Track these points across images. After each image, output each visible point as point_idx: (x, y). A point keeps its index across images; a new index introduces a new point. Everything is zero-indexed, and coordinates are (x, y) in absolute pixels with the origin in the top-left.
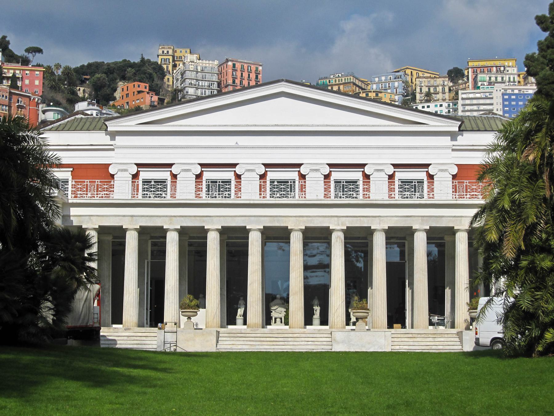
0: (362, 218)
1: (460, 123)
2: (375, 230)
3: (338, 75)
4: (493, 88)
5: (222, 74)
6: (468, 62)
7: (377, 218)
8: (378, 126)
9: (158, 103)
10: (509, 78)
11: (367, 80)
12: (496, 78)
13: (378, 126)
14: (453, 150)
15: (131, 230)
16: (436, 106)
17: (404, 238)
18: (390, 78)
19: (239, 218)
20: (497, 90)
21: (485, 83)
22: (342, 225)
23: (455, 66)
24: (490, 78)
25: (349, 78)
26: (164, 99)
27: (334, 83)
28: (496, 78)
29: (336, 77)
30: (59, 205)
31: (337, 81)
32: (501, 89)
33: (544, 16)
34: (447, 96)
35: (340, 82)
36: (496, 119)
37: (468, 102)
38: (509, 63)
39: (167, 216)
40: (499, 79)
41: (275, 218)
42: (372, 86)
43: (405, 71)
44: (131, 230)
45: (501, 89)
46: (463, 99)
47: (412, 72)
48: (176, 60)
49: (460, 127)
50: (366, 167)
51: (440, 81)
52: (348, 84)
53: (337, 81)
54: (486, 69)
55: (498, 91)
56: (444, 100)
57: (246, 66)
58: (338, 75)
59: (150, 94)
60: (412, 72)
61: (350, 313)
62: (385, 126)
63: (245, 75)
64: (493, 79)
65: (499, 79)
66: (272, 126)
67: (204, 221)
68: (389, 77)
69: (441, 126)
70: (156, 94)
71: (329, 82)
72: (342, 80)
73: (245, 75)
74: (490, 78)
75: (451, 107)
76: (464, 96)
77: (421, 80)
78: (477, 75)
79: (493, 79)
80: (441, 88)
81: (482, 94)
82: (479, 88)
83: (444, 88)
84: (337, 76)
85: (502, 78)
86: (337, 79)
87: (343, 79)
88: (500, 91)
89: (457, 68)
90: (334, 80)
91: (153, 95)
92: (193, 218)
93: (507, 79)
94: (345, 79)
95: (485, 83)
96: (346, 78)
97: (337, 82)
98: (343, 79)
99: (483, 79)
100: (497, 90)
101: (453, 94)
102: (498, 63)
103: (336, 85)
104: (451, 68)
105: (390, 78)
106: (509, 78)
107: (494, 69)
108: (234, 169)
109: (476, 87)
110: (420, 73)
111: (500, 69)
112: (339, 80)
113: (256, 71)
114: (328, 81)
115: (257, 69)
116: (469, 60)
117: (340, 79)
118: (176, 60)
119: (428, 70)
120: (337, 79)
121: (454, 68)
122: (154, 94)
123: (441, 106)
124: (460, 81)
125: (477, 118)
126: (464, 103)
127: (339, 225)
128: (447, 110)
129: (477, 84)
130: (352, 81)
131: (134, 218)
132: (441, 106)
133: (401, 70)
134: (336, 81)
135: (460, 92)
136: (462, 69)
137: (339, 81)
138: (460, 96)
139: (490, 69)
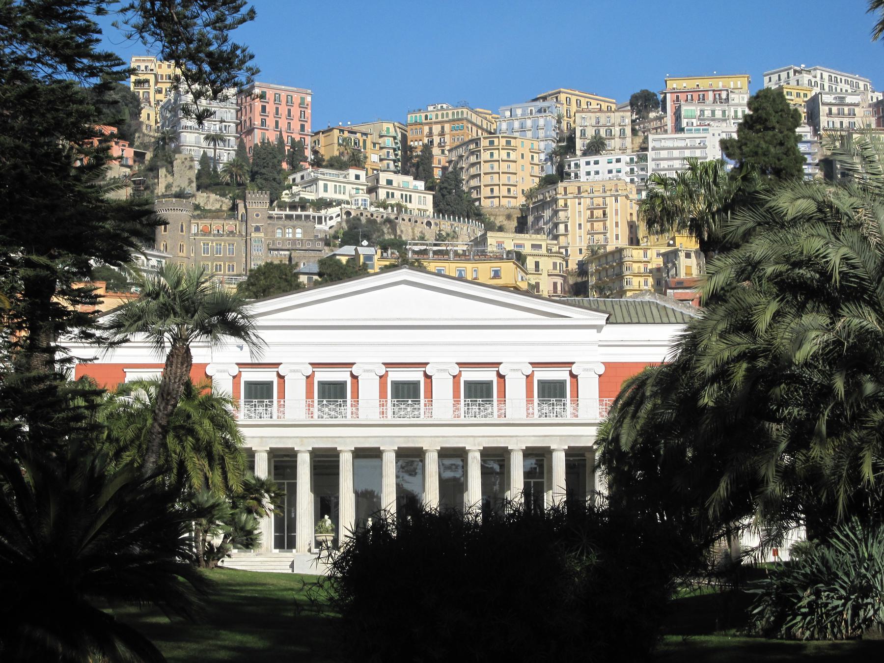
0: (499, 438)
1: (607, 316)
2: (512, 450)
3: (442, 107)
4: (708, 130)
5: (244, 110)
6: (666, 81)
7: (514, 438)
8: (514, 319)
9: (135, 161)
10: (736, 112)
11: (490, 112)
12: (713, 112)
13: (514, 319)
14: (600, 346)
15: (389, 451)
17: (543, 455)
18: (531, 111)
19: (373, 439)
20: (713, 135)
21: (694, 121)
23: (644, 88)
24: (702, 111)
25: (460, 111)
26: (144, 154)
27: (434, 120)
28: (713, 112)
29: (438, 110)
32: (720, 132)
33: (731, 140)
34: (628, 141)
35: (445, 119)
36: (651, 304)
37: (664, 154)
38: (735, 84)
39: (297, 437)
40: (719, 114)
41: (410, 439)
42: (500, 125)
43: (557, 98)
44: (389, 451)
45: (720, 132)
46: (654, 149)
47: (822, 74)
48: (160, 81)
49: (608, 319)
51: (616, 117)
52: (458, 122)
54: (695, 95)
55: (717, 135)
56: (623, 150)
57: (283, 94)
58: (442, 107)
59: (121, 144)
60: (822, 74)
63: (283, 110)
64: (708, 113)
65: (719, 114)
67: (336, 443)
68: (529, 109)
69: (586, 319)
70: (131, 145)
71: (426, 118)
72: (447, 114)
73: (283, 110)
74: (702, 111)
76: (657, 145)
78: (680, 107)
79: (708, 113)
80: (618, 129)
81: (687, 140)
82: (682, 130)
83: (624, 130)
84: (439, 107)
85: (724, 112)
86: (440, 113)
87: (450, 112)
88: (719, 135)
89: (647, 91)
90: (434, 114)
91: (124, 146)
92: (325, 439)
93: (732, 114)
94: (453, 113)
95: (694, 121)
96: (455, 111)
97: (440, 119)
99: (690, 114)
100: (713, 135)
101: (639, 140)
102: (720, 84)
103: (436, 123)
104: (637, 90)
105: (531, 111)
106: (736, 112)
107: (711, 94)
109: (679, 129)
110: (582, 99)
111: (720, 95)
112: (443, 114)
113: (300, 104)
114: (423, 115)
115: (303, 99)
116: (668, 77)
117: (445, 112)
118: (160, 81)
119: (597, 95)
120: (440, 113)
121: (643, 92)
122: (127, 145)
123: (618, 161)
124: (652, 115)
125: (629, 304)
126: (657, 157)
127: (475, 445)
128: (628, 169)
129: (680, 122)
130: (465, 116)
131: (264, 439)
133: (550, 95)
134: (437, 116)
135: (651, 137)
136: (656, 92)
137: (443, 117)
138: (651, 145)
139: (704, 95)
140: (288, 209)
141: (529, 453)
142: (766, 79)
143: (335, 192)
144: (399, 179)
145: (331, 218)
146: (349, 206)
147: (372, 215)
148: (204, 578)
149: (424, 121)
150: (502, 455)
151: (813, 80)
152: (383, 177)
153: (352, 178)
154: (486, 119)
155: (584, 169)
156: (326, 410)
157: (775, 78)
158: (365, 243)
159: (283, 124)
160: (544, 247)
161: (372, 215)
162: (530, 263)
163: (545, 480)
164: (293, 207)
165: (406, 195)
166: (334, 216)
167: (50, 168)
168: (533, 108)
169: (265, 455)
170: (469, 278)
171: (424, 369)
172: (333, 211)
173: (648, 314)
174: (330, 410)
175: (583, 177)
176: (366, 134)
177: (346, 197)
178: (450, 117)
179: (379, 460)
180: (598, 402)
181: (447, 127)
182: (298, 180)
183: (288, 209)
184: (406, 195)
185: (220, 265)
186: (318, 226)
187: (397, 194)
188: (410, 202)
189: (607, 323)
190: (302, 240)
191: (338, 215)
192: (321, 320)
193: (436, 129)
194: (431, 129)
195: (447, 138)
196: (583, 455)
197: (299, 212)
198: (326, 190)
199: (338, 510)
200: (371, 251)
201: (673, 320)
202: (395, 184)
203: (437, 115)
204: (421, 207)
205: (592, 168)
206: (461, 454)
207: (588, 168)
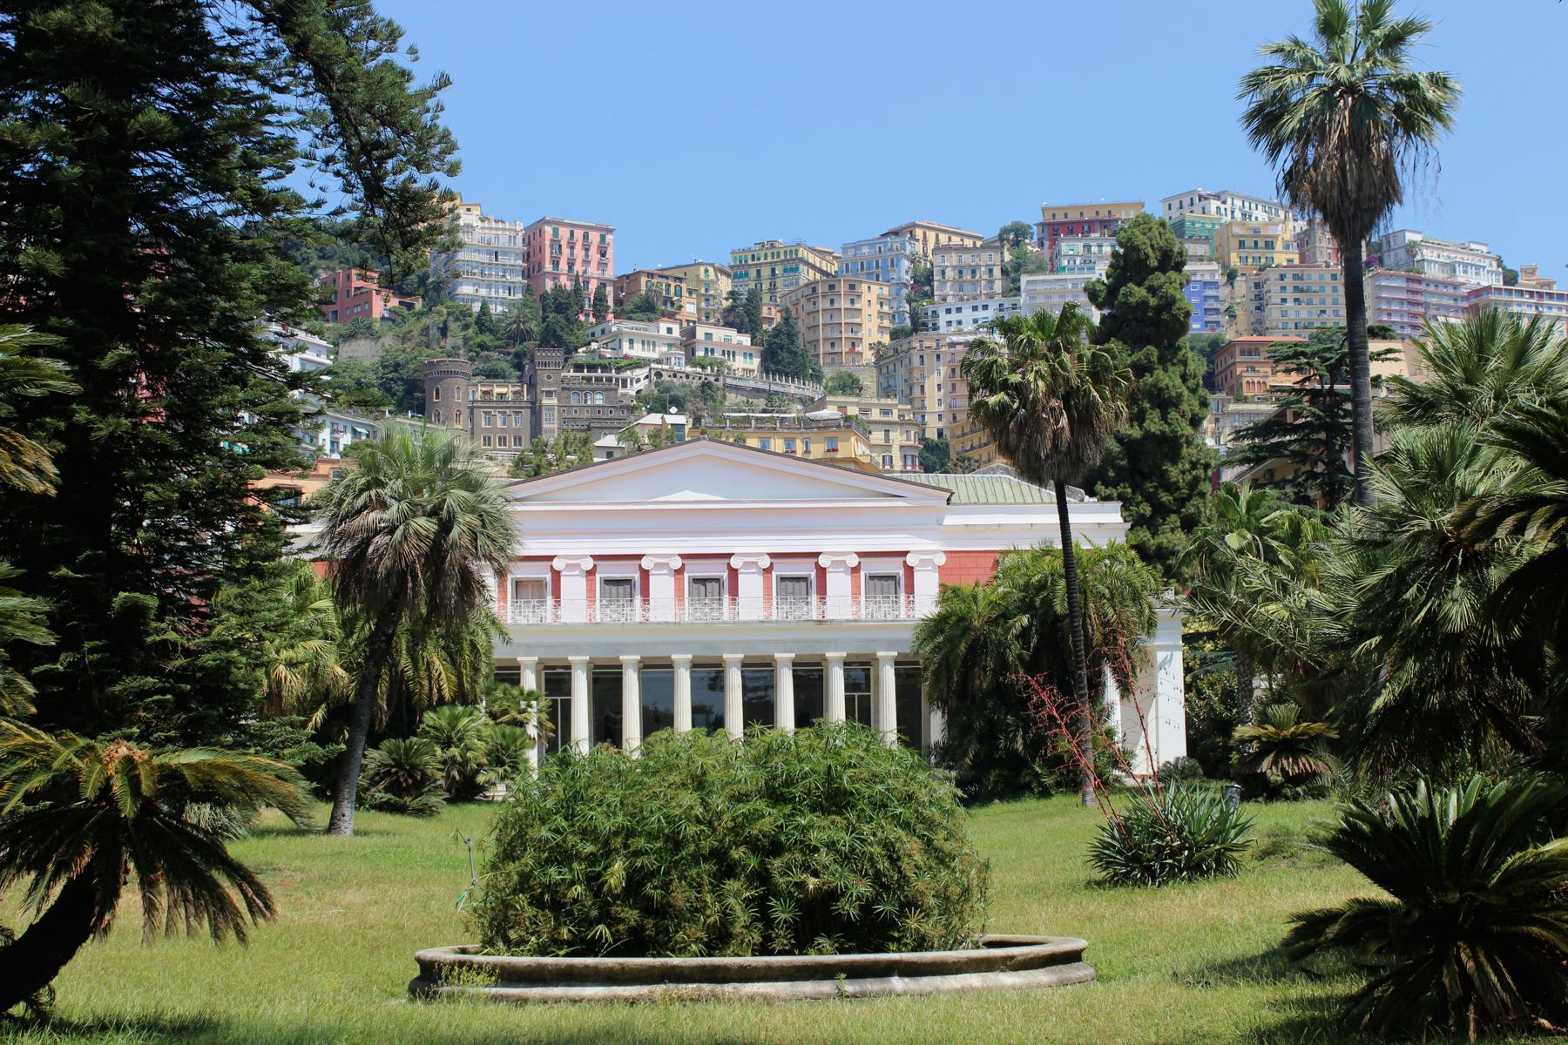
16: (975, 308)
17: (868, 664)
49: (948, 500)
71: (753, 259)
97: (769, 260)
144: (720, 334)
145: (638, 381)
146: (659, 366)
148: (756, 968)
149: (750, 262)
151: (1223, 207)
152: (701, 332)
153: (663, 332)
156: (608, 611)
158: (674, 410)
160: (895, 412)
163: (872, 694)
164: (592, 368)
166: (642, 377)
167: (199, 579)
172: (641, 373)
173: (981, 492)
175: (943, 328)
176: (680, 279)
178: (782, 257)
182: (598, 333)
186: (621, 390)
193: (766, 272)
194: (759, 272)
195: (779, 283)
199: (595, 721)
200: (681, 419)
202: (715, 339)
203: (766, 255)
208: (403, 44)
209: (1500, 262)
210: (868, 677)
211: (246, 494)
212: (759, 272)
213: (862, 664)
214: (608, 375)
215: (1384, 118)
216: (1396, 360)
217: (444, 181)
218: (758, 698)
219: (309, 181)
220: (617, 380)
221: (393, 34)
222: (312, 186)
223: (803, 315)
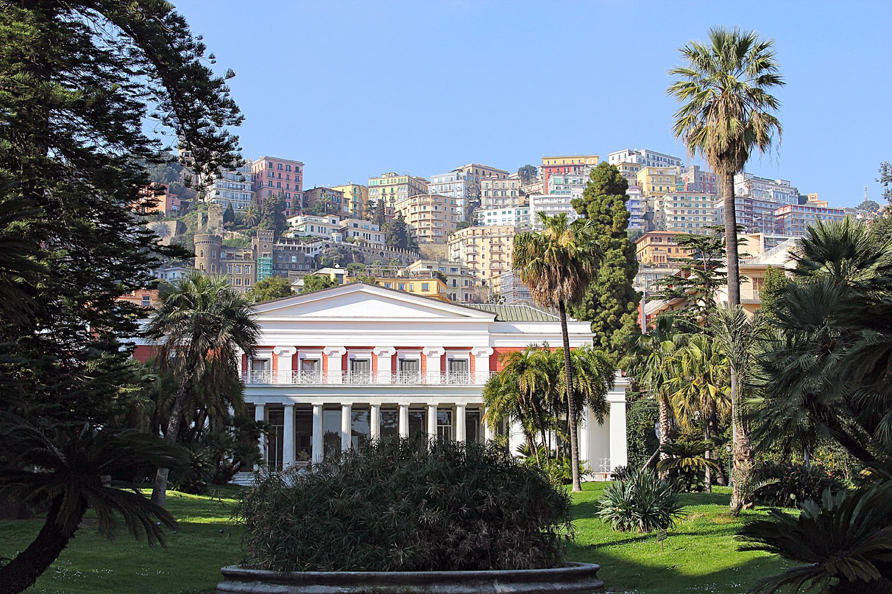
2: (285, 406)
15: (259, 405)
16: (504, 213)
17: (450, 409)
18: (452, 178)
22: (407, 401)
27: (386, 184)
30: (567, 552)
31: (390, 181)
44: (259, 405)
47: (484, 172)
50: (424, 349)
53: (390, 181)
59: (172, 197)
60: (484, 172)
61: (128, 69)
62: (435, 318)
66: (353, 317)
75: (521, 214)
77: (487, 182)
86: (390, 179)
90: (386, 180)
95: (562, 186)
97: (390, 184)
98: (397, 179)
105: (452, 178)
108: (322, 351)
114: (379, 181)
120: (390, 179)
123: (510, 212)
132: (510, 212)
140: (286, 243)
141: (440, 408)
142: (611, 158)
143: (319, 232)
146: (327, 241)
147: (344, 247)
149: (379, 184)
150: (423, 409)
154: (420, 183)
155: (487, 218)
157: (616, 157)
159: (284, 185)
161: (344, 247)
162: (450, 281)
165: (322, 232)
168: (453, 177)
169: (262, 408)
170: (408, 291)
171: (322, 351)
173: (524, 315)
174: (307, 377)
177: (326, 235)
178: (397, 183)
179: (340, 412)
180: (440, 373)
181: (395, 189)
183: (286, 243)
184: (322, 232)
185: (240, 280)
187: (361, 234)
188: (370, 239)
189: (495, 321)
190: (296, 264)
191: (321, 247)
192: (387, 318)
193: (388, 190)
194: (384, 190)
196: (478, 409)
197: (294, 245)
198: (312, 230)
201: (541, 319)
204: (377, 242)
205: (492, 217)
206: (395, 408)
207: (489, 217)
208: (206, 53)
209: (796, 192)
210: (450, 417)
211: (85, 304)
212: (384, 190)
213: (446, 409)
214: (299, 246)
215: (116, 184)
216: (745, 245)
217: (233, 130)
218: (128, 337)
219: (153, 130)
220: (304, 248)
221: (201, 49)
222: (162, 133)
223: (409, 215)
